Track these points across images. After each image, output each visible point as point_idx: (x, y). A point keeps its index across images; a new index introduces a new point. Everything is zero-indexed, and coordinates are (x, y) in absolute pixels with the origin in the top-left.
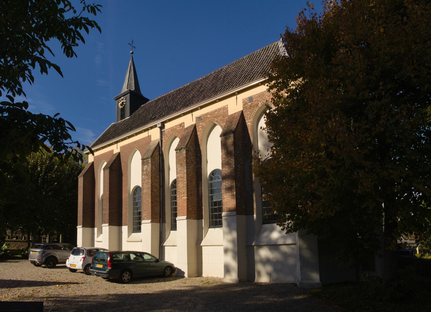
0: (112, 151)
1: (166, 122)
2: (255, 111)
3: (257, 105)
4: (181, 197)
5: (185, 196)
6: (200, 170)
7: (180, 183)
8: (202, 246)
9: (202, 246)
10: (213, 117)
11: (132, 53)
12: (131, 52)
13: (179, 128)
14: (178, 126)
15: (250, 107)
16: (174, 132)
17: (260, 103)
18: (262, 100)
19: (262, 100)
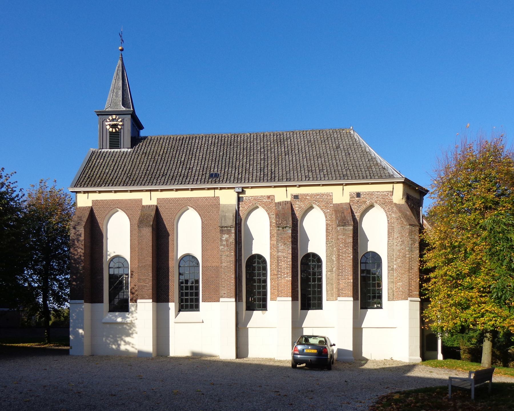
0: (141, 200)
1: (247, 188)
2: (363, 207)
3: (365, 202)
4: (284, 277)
5: (289, 277)
6: (296, 251)
7: (282, 262)
8: (248, 328)
9: (248, 328)
10: (314, 200)
11: (122, 50)
12: (120, 48)
13: (266, 200)
14: (265, 198)
15: (358, 202)
16: (259, 202)
17: (368, 201)
18: (370, 199)
19: (370, 199)
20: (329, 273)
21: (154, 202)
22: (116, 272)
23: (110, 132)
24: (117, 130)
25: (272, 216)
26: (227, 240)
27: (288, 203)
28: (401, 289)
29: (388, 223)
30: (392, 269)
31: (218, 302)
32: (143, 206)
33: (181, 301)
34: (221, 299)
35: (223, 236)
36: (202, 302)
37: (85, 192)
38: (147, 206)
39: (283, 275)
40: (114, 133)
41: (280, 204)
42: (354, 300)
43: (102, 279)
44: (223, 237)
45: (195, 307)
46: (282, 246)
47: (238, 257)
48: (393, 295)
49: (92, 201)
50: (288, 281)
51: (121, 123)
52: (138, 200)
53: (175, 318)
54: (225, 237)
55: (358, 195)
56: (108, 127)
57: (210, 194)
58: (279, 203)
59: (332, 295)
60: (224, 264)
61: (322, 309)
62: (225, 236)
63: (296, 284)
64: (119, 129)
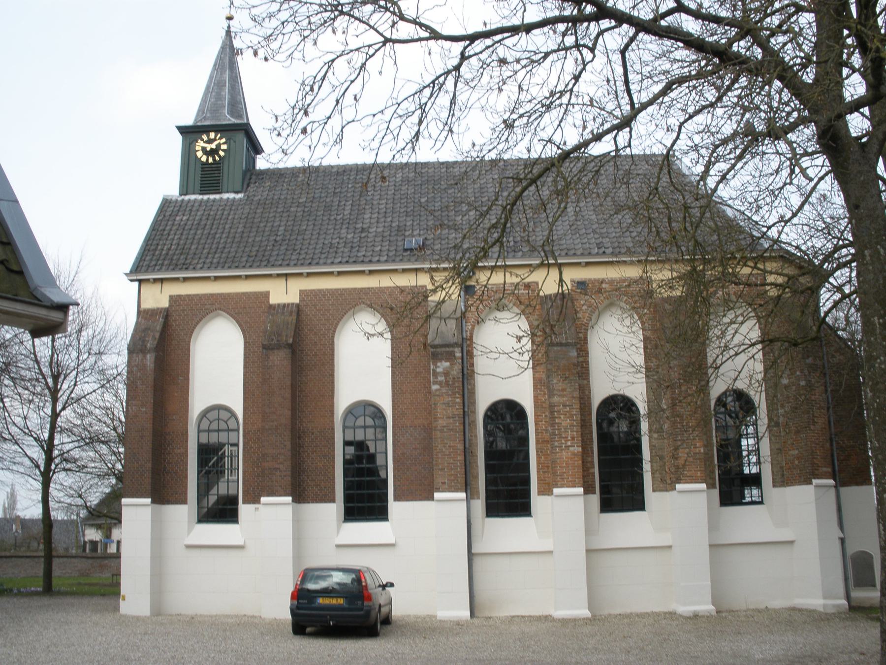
0: (266, 295)
20: (655, 435)
21: (293, 298)
22: (214, 438)
23: (203, 163)
24: (217, 158)
26: (446, 374)
28: (796, 462)
30: (777, 424)
31: (773, 482)
34: (437, 495)
35: (439, 364)
36: (654, 491)
38: (279, 305)
39: (563, 441)
42: (586, 492)
43: (186, 454)
44: (439, 367)
46: (560, 384)
47: (468, 406)
48: (783, 475)
50: (574, 454)
54: (442, 367)
56: (199, 154)
59: (663, 480)
60: (440, 421)
62: (444, 365)
63: (589, 459)
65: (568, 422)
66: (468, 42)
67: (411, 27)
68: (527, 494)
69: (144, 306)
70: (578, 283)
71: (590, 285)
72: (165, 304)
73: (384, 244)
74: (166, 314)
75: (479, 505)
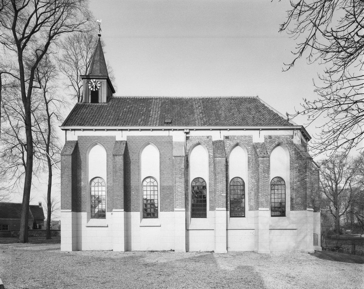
21: (125, 139)
25: (210, 151)
27: (221, 142)
29: (290, 157)
32: (116, 141)
33: (193, 210)
37: (72, 130)
40: (94, 91)
41: (216, 142)
45: (204, 215)
49: (78, 136)
51: (99, 85)
52: (113, 137)
53: (87, 223)
55: (270, 137)
57: (166, 133)
58: (216, 142)
61: (206, 217)
64: (98, 89)
65: (222, 186)
66: (24, 5)
67: (65, 18)
68: (205, 210)
69: (68, 140)
70: (226, 137)
71: (302, 208)
72: (76, 139)
73: (157, 121)
74: (77, 144)
75: (189, 213)
